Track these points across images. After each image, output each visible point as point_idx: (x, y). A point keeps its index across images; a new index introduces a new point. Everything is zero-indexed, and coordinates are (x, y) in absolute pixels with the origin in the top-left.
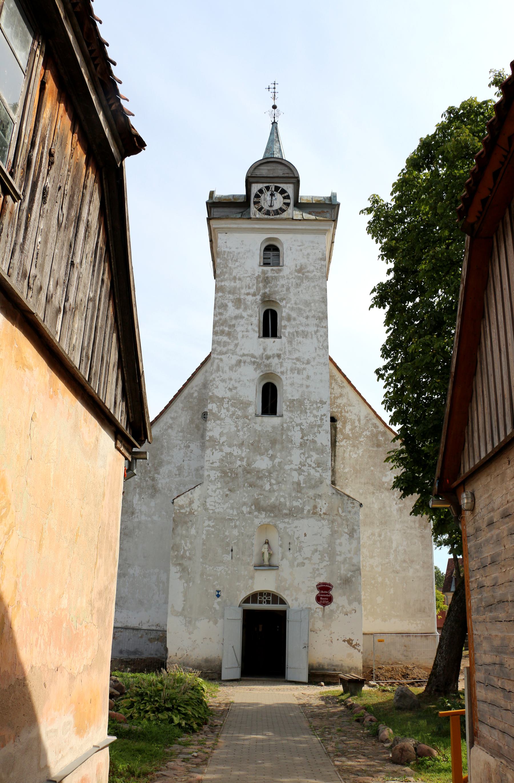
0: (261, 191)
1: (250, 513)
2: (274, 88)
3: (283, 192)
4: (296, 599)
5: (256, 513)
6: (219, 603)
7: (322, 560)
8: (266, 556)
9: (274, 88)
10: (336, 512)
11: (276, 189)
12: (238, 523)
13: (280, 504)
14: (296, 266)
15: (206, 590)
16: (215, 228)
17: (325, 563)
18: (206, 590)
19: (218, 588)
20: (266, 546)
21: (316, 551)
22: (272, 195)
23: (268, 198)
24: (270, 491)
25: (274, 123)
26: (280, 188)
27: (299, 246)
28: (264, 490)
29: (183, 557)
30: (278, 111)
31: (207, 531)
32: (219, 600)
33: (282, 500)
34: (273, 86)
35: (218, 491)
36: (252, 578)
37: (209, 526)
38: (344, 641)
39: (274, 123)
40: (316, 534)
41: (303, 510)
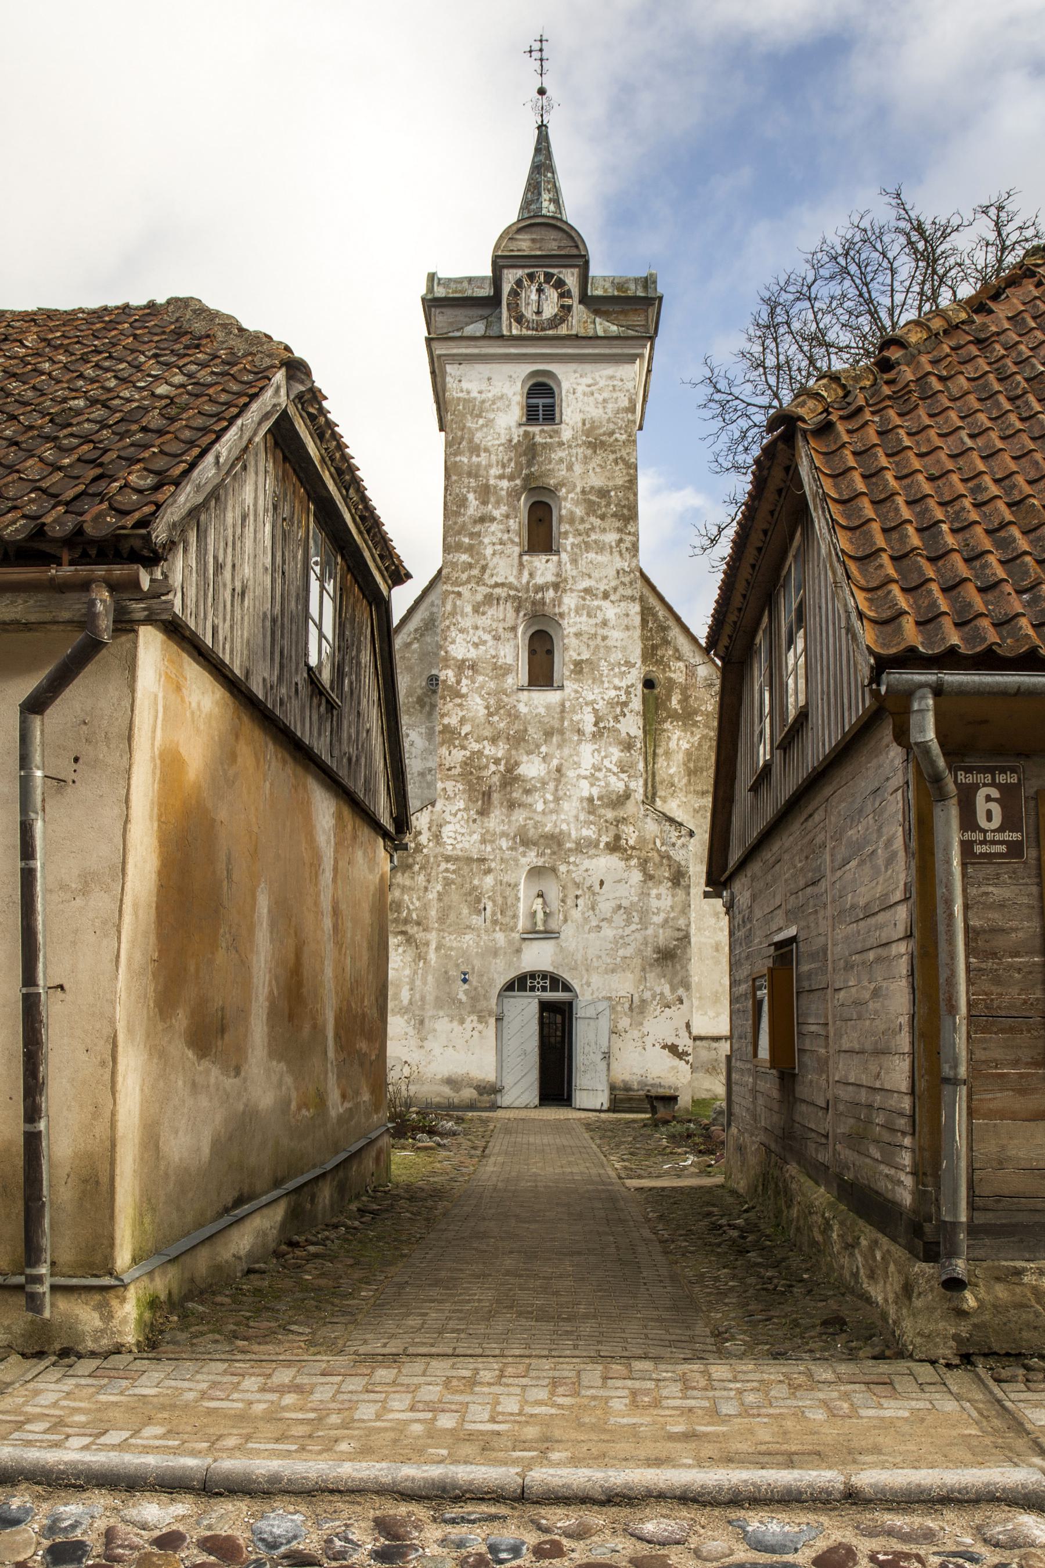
0: (519, 283)
1: (512, 849)
2: (541, 50)
3: (560, 284)
4: (588, 984)
5: (521, 849)
6: (466, 992)
7: (628, 922)
8: (540, 915)
9: (541, 50)
10: (651, 846)
11: (548, 277)
12: (493, 865)
13: (561, 832)
14: (584, 424)
15: (446, 972)
16: (440, 356)
17: (633, 927)
18: (446, 972)
19: (463, 968)
20: (540, 900)
21: (620, 907)
22: (540, 291)
23: (534, 296)
24: (544, 812)
25: (542, 128)
26: (553, 275)
27: (589, 386)
28: (535, 811)
29: (406, 922)
30: (549, 100)
31: (445, 878)
32: (466, 986)
33: (564, 827)
34: (536, 46)
35: (459, 815)
36: (518, 951)
37: (447, 870)
38: (664, 1047)
39: (542, 128)
40: (619, 881)
41: (598, 842)
